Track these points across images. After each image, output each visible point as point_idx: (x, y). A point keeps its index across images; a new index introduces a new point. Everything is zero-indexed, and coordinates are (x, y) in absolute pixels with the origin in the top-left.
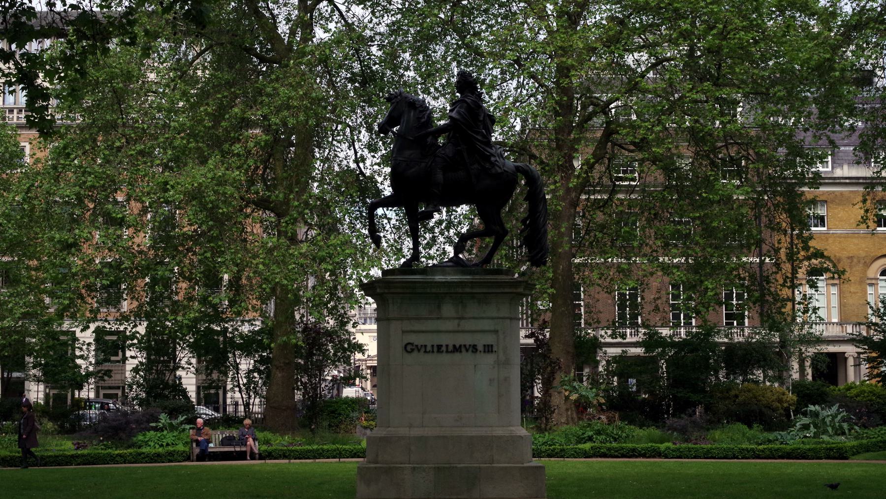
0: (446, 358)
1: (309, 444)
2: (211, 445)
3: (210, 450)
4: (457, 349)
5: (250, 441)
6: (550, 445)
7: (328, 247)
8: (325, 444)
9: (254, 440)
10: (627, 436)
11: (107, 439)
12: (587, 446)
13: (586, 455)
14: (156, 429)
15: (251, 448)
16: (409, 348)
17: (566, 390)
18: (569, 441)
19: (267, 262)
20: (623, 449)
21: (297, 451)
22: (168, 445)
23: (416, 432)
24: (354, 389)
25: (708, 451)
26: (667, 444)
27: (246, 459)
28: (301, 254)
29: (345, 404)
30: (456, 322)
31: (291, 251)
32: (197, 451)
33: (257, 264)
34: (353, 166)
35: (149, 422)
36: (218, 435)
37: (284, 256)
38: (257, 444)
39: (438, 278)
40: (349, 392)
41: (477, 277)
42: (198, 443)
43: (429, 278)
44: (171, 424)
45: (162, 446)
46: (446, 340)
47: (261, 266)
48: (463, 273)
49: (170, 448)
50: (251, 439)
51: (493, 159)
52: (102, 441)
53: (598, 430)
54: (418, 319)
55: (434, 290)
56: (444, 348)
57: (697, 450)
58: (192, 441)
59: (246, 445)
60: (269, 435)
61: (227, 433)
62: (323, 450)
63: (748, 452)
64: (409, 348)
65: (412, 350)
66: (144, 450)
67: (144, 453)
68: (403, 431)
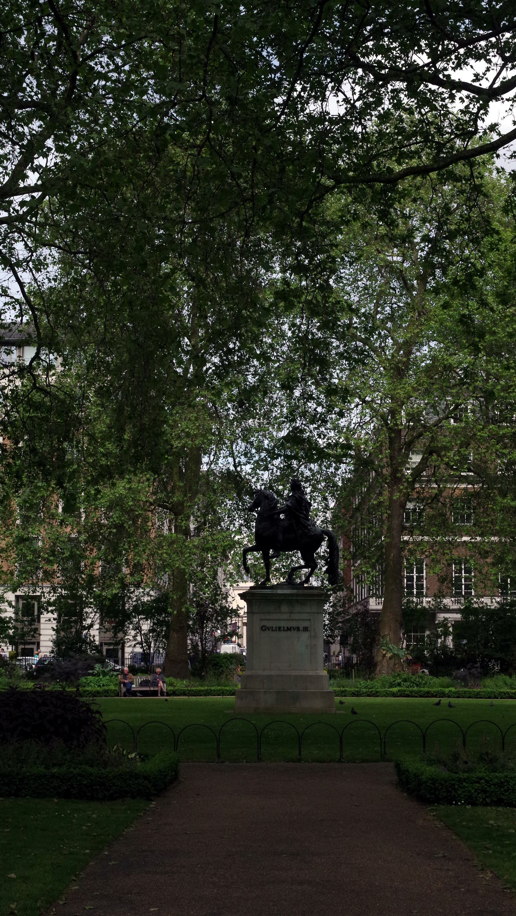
0: (283, 634)
1: (202, 686)
2: (134, 686)
3: (133, 689)
4: (289, 629)
5: (161, 684)
6: (369, 689)
7: (214, 540)
8: (213, 686)
9: (163, 682)
10: (426, 684)
11: (62, 681)
12: (395, 689)
13: (394, 695)
14: (92, 675)
15: (161, 688)
16: (264, 628)
17: (384, 650)
18: (384, 686)
19: (169, 552)
20: (420, 691)
21: (193, 691)
22: (103, 685)
23: (267, 673)
24: (232, 645)
25: (478, 693)
26: (450, 689)
27: (157, 696)
28: (194, 545)
29: (225, 658)
30: (289, 615)
31: (186, 544)
32: (124, 690)
33: (162, 554)
34: (232, 468)
35: (87, 669)
36: (138, 679)
37: (181, 547)
38: (165, 685)
39: (280, 591)
40: (226, 649)
41: (300, 591)
42: (125, 684)
43: (274, 591)
44: (103, 672)
45: (99, 686)
46: (283, 624)
47: (165, 555)
48: (293, 589)
49: (106, 688)
50: (161, 682)
51: (309, 527)
52: (59, 682)
53: (405, 679)
54: (269, 613)
55: (277, 598)
56: (282, 629)
57: (470, 693)
58: (120, 683)
59: (158, 686)
60: (172, 679)
61: (144, 678)
62: (211, 690)
63: (505, 694)
64: (264, 628)
65: (265, 629)
66: (87, 688)
67: (88, 691)
68: (260, 672)
